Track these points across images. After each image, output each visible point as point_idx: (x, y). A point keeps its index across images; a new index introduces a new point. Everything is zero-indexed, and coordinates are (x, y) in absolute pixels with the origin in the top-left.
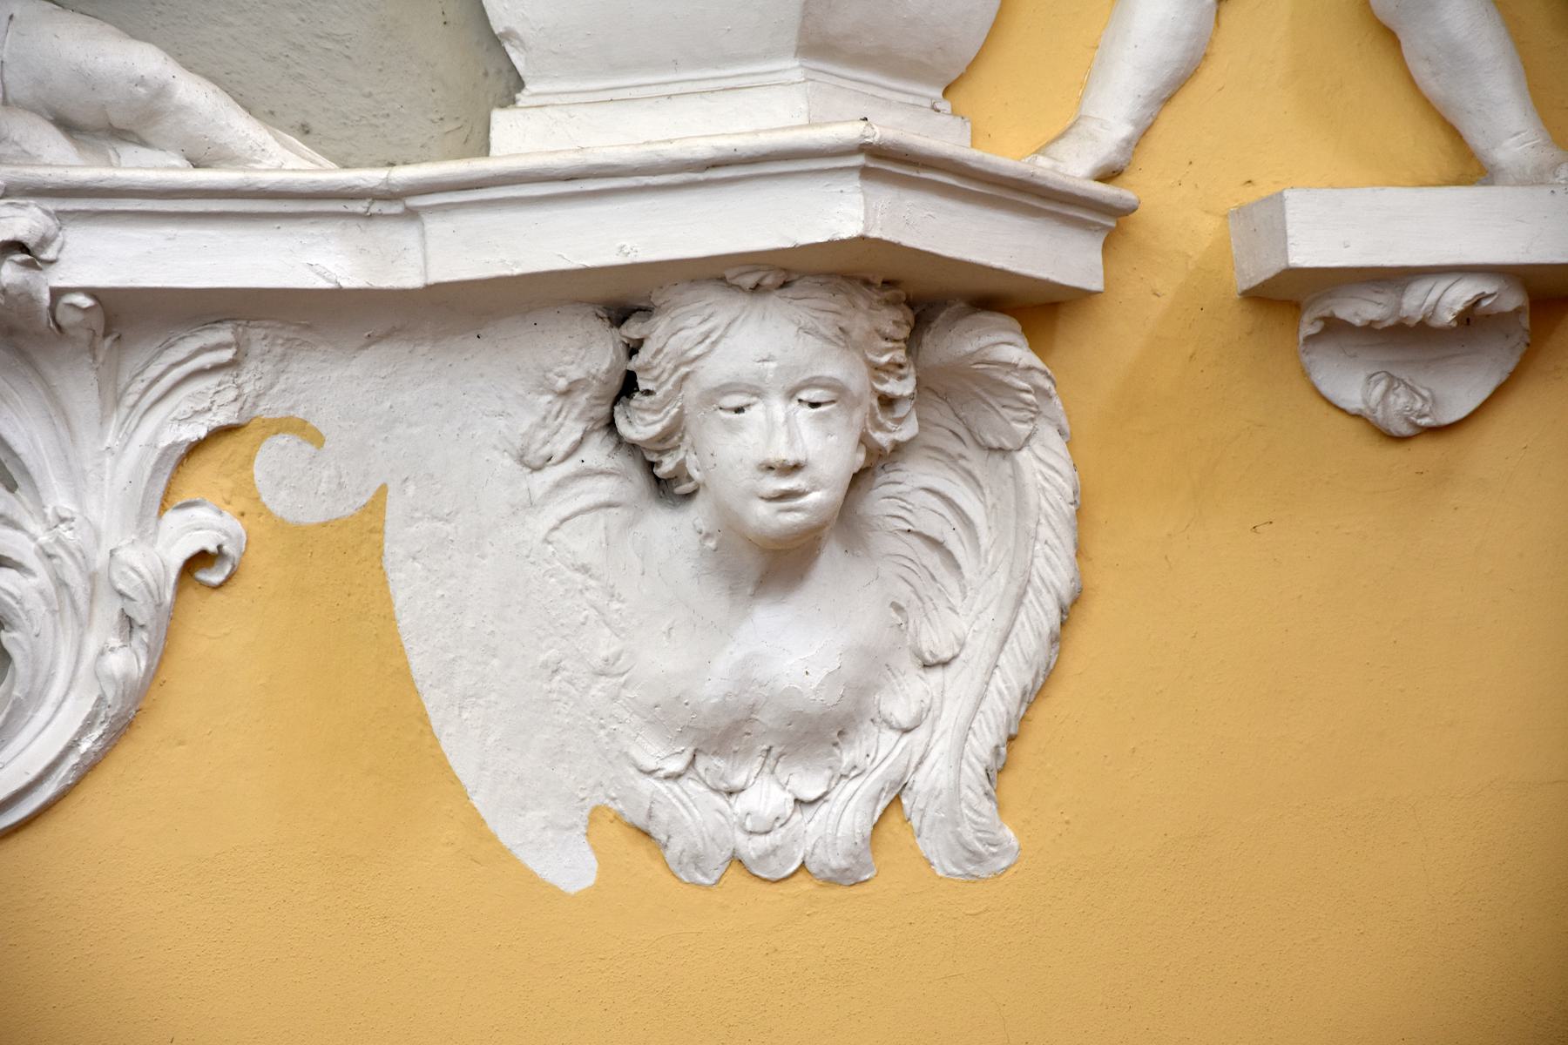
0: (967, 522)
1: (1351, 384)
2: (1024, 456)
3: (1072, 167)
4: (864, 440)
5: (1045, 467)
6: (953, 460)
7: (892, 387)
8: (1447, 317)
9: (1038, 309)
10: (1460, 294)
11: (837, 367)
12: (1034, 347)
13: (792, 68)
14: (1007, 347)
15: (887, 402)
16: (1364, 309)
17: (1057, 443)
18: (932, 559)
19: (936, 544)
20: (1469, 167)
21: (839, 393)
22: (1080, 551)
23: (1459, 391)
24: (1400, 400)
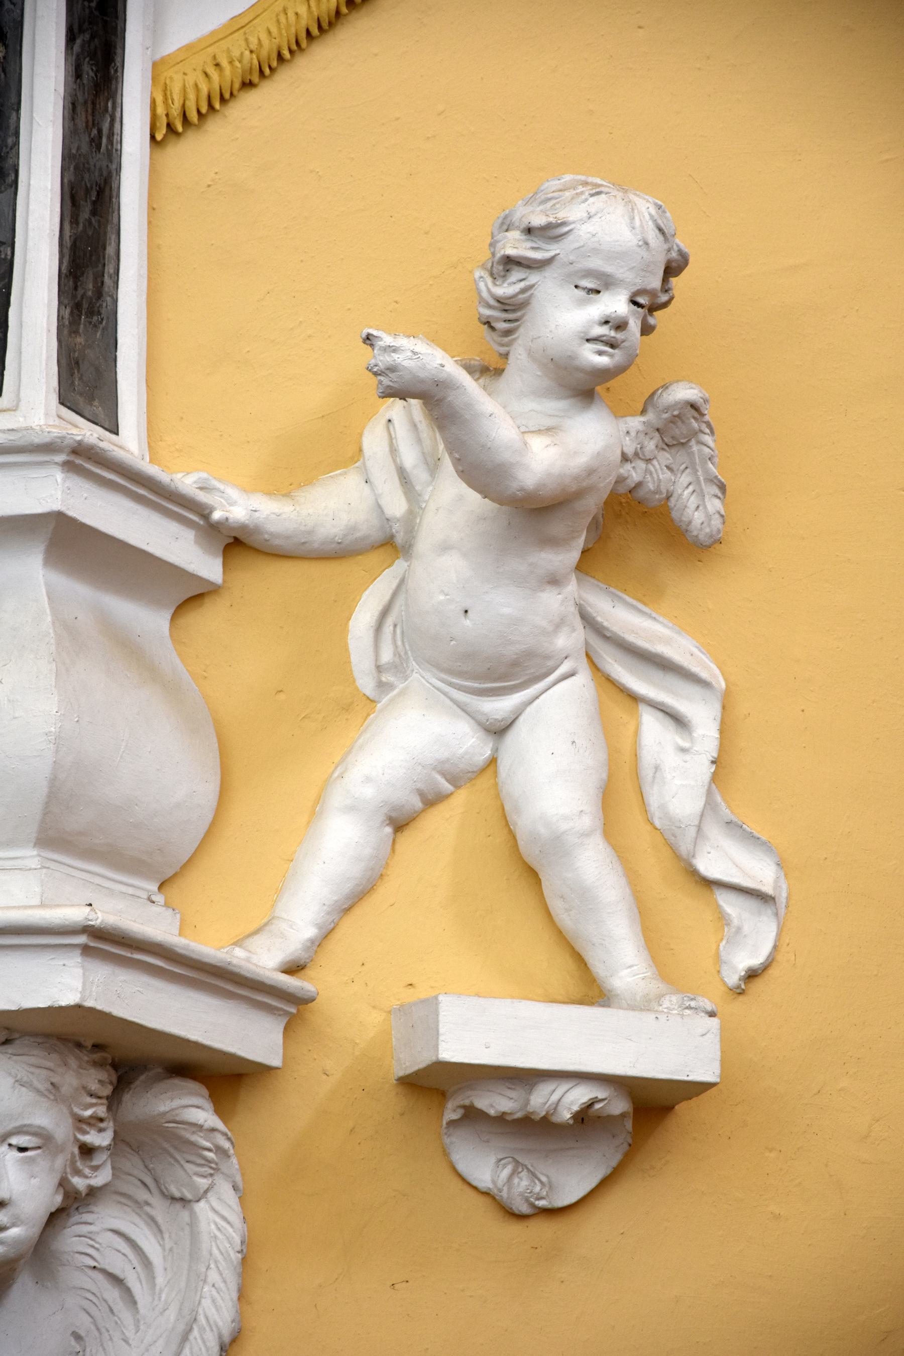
0: (147, 1263)
1: (483, 1165)
2: (201, 1207)
3: (264, 959)
4: (63, 1183)
5: (219, 1218)
6: (139, 1206)
7: (93, 1138)
8: (565, 1115)
9: (225, 1079)
10: (576, 1097)
11: (45, 1117)
12: (219, 1111)
13: (30, 856)
14: (194, 1109)
15: (87, 1151)
16: (498, 1102)
17: (231, 1197)
18: (112, 1294)
19: (117, 1280)
20: (591, 991)
21: (46, 1140)
22: (242, 1295)
23: (572, 1180)
24: (522, 1183)
